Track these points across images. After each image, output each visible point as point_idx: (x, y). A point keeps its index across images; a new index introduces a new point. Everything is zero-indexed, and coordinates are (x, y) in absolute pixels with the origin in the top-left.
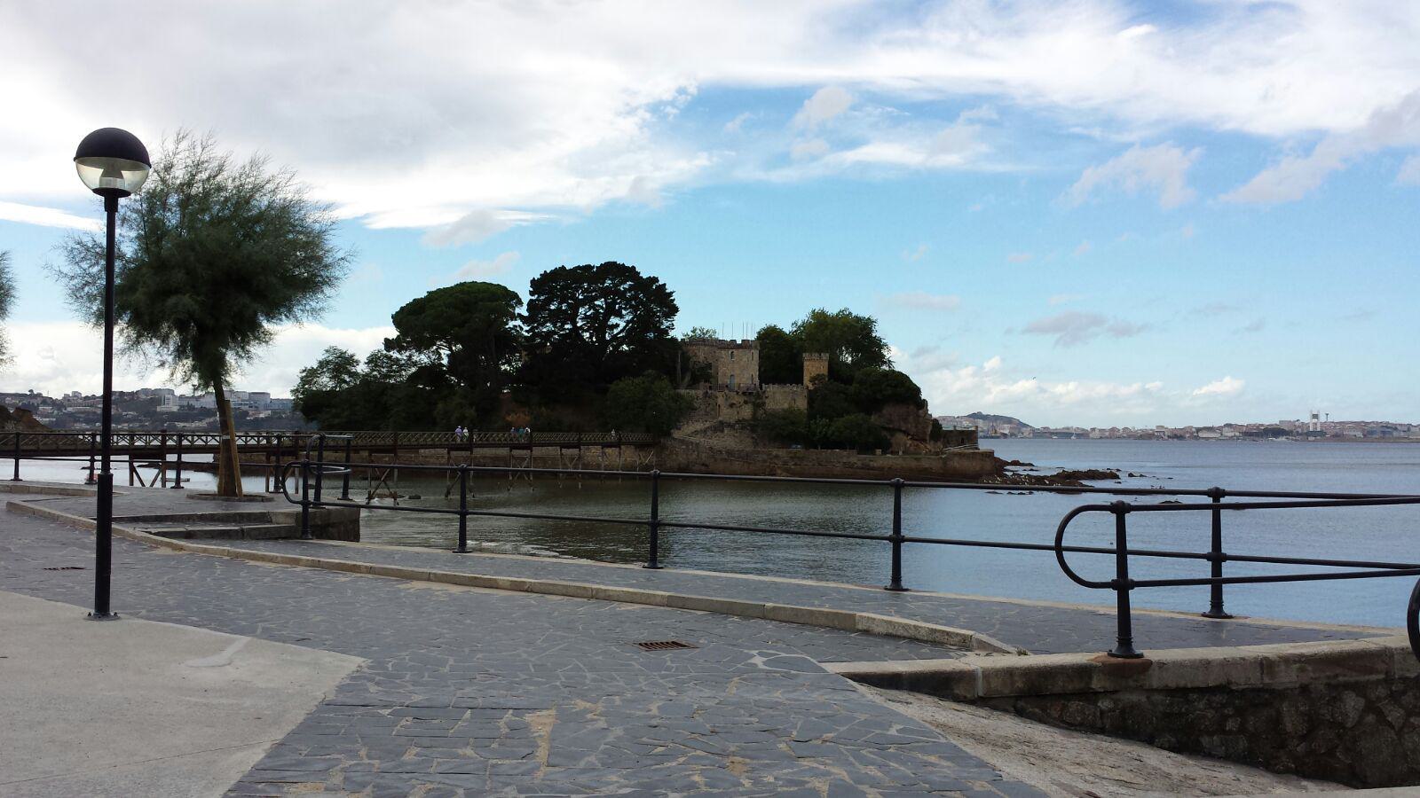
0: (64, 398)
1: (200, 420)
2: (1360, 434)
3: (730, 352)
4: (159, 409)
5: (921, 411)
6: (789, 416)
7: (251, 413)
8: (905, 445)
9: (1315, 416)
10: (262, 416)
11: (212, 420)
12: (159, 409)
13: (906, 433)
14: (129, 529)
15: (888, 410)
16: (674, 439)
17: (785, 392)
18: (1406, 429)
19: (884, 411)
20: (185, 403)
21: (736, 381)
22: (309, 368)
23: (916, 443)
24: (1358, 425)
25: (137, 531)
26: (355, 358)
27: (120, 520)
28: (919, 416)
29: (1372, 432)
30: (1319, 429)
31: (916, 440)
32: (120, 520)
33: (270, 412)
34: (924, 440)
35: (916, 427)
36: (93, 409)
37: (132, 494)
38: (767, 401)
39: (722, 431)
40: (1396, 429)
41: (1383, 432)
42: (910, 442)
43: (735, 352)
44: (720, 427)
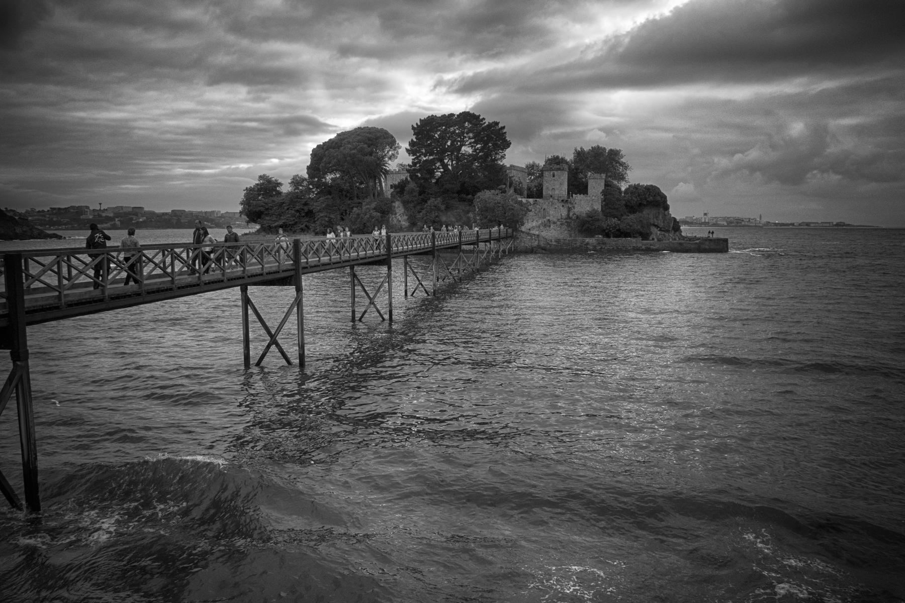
0: (26, 212)
1: (106, 223)
2: (725, 224)
3: (552, 173)
4: (81, 217)
5: (666, 212)
6: (592, 216)
7: (134, 218)
8: (657, 234)
9: (705, 214)
10: (141, 220)
11: (113, 223)
12: (81, 217)
13: (657, 226)
14: (54, 431)
15: (646, 212)
16: (521, 231)
17: (587, 200)
18: (748, 220)
19: (644, 212)
20: (96, 214)
21: (557, 192)
22: (248, 187)
23: (663, 233)
24: (724, 219)
25: (33, 356)
26: (279, 181)
27: (34, 392)
28: (665, 215)
29: (731, 222)
30: (707, 221)
31: (664, 231)
32: (34, 392)
33: (145, 218)
34: (668, 231)
35: (664, 222)
36: (43, 218)
37: (103, 367)
38: (576, 206)
39: (550, 226)
40: (743, 221)
41: (737, 223)
42: (659, 232)
43: (556, 173)
44: (547, 225)
